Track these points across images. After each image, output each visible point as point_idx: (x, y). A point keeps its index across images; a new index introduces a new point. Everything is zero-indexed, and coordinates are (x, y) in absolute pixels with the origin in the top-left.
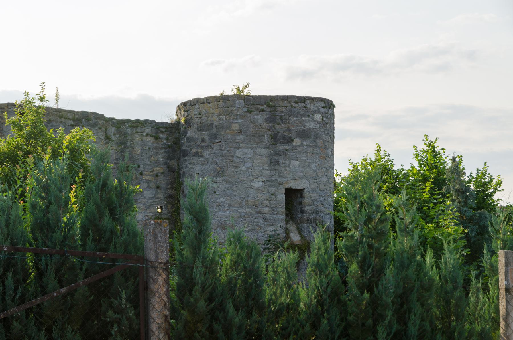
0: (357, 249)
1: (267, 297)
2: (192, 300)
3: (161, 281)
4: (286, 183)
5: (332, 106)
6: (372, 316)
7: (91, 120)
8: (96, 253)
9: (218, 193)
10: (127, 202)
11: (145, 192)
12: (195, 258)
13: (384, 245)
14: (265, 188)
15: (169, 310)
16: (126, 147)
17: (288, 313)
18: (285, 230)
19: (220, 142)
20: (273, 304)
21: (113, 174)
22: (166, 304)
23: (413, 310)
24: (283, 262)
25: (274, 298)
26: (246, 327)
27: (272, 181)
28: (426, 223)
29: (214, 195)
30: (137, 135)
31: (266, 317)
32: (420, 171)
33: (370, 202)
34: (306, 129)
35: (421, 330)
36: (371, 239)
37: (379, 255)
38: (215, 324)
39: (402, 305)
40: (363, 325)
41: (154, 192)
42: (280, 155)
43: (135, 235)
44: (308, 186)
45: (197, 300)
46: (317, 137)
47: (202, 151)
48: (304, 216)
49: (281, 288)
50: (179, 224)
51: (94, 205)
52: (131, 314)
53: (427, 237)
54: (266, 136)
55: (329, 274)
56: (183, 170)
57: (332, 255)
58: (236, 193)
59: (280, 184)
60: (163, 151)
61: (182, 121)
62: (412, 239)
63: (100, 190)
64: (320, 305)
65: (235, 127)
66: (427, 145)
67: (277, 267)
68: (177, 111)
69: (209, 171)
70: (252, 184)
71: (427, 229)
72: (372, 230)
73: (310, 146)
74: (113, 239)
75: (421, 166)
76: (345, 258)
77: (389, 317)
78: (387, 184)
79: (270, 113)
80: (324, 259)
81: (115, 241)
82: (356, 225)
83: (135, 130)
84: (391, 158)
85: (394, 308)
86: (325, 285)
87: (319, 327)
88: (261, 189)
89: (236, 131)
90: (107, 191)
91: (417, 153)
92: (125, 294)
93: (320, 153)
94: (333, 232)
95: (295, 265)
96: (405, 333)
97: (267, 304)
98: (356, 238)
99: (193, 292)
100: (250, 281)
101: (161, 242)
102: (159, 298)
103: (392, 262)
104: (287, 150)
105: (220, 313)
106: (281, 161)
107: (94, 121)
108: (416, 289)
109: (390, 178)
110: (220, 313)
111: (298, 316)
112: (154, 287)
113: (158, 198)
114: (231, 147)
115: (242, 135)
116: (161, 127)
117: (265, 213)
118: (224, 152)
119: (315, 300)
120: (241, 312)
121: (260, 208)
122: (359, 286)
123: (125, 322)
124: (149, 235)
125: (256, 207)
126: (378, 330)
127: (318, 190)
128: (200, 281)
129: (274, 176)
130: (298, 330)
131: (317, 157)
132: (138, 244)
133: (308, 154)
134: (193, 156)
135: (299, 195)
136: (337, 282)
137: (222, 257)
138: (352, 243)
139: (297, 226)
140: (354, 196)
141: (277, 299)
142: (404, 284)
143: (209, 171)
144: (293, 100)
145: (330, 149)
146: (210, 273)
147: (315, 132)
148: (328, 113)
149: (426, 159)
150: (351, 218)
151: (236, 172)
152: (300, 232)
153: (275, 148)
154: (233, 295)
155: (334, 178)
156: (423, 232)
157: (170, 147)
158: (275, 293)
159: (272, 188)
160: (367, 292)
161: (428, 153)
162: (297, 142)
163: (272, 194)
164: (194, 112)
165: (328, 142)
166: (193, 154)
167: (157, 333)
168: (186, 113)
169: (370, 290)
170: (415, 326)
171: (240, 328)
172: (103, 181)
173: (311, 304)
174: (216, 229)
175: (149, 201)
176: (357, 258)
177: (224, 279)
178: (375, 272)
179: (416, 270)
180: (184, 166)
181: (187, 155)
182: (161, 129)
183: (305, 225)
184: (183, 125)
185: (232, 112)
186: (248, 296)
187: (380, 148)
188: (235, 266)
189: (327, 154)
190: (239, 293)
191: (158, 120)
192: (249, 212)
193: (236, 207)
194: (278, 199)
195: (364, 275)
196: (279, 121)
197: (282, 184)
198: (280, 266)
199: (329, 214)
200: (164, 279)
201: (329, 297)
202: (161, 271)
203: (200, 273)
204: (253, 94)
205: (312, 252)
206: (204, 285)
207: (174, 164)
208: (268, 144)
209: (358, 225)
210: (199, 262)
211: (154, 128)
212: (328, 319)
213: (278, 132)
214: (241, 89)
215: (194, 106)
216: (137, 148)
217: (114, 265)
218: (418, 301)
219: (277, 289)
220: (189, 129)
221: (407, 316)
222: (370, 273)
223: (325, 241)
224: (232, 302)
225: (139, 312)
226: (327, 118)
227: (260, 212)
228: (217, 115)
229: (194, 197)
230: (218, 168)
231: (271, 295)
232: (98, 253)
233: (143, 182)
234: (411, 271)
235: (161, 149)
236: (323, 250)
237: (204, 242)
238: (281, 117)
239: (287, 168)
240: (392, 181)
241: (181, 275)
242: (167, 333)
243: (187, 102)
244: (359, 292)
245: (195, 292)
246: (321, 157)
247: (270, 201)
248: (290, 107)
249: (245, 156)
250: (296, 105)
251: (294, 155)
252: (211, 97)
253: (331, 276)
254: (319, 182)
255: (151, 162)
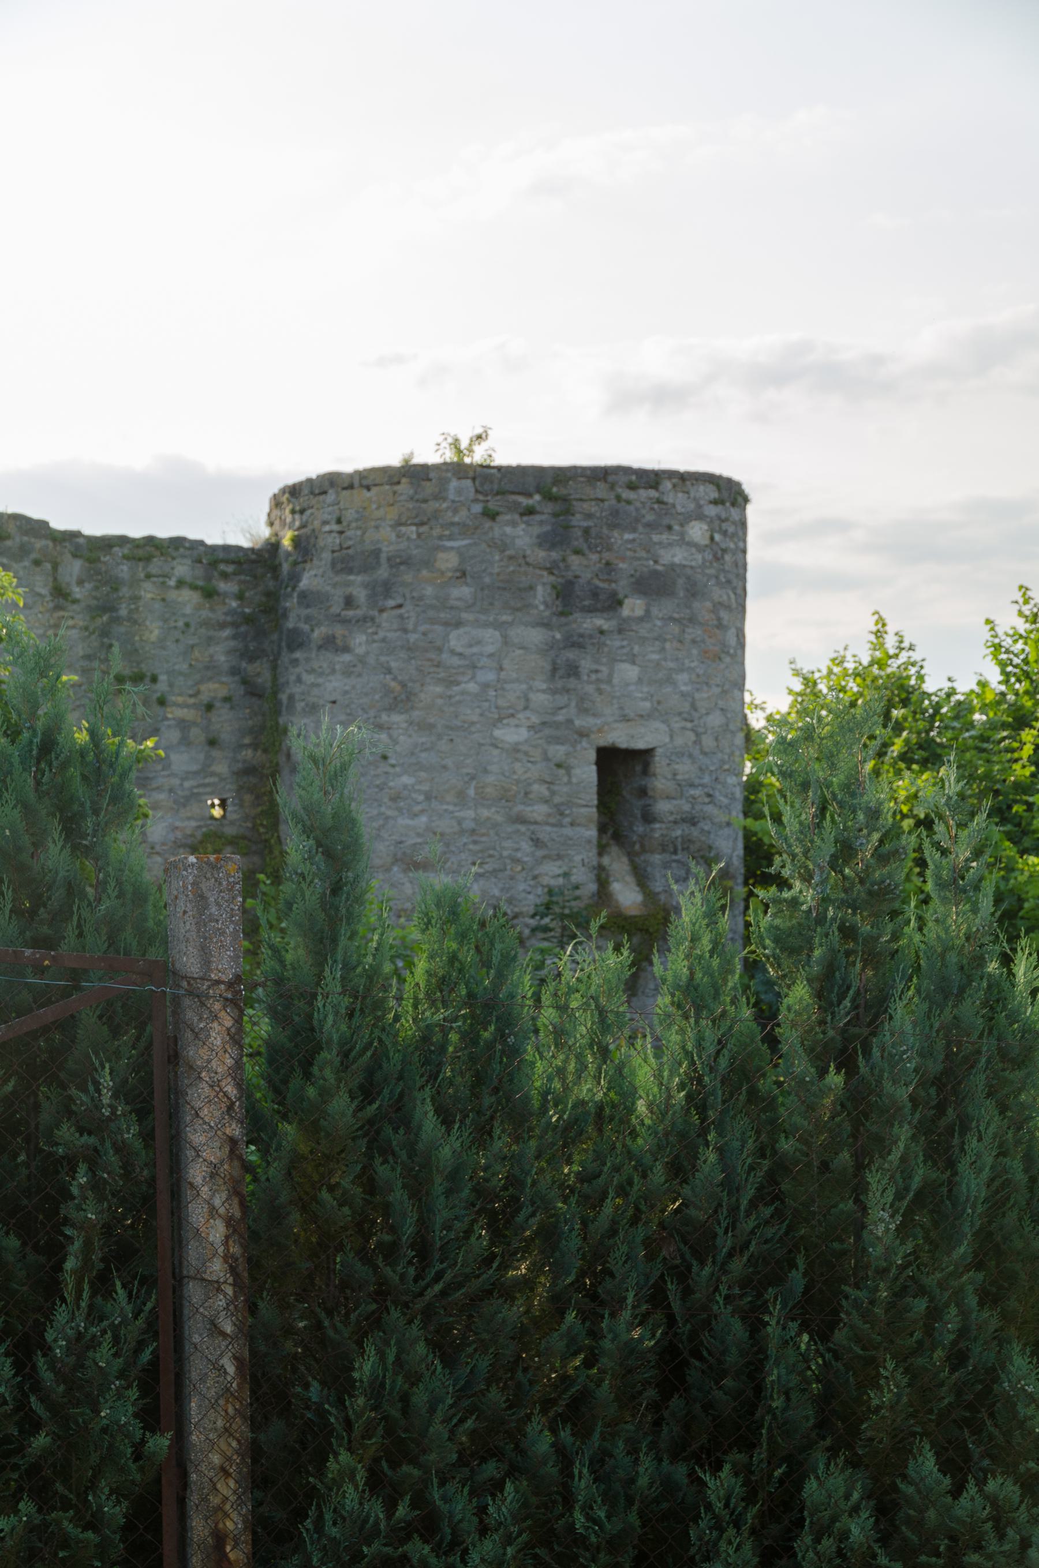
0: (809, 941)
1: (538, 1084)
2: (311, 1092)
3: (217, 1037)
4: (600, 731)
5: (740, 500)
6: (851, 1140)
7: (8, 537)
8: (23, 952)
9: (393, 761)
10: (115, 799)
11: (174, 757)
12: (320, 964)
13: (890, 927)
14: (535, 747)
15: (242, 1123)
16: (117, 620)
17: (600, 1130)
18: (595, 872)
19: (400, 606)
20: (556, 1105)
21: (78, 703)
22: (233, 1103)
23: (974, 1124)
24: (585, 979)
25: (557, 1085)
26: (474, 1171)
27: (557, 725)
28: (1022, 853)
29: (384, 767)
30: (148, 585)
31: (533, 1143)
32: (1003, 694)
33: (847, 799)
34: (659, 568)
35: (997, 1183)
36: (850, 911)
37: (872, 958)
38: (382, 1164)
39: (941, 1108)
40: (825, 1166)
41: (202, 756)
42: (581, 646)
43: (140, 897)
44: (667, 740)
45: (325, 1094)
46: (694, 592)
47: (346, 633)
48: (653, 830)
49: (580, 1057)
50: (276, 853)
51: (15, 806)
52: (130, 1132)
53: (1023, 896)
54: (540, 588)
55: (724, 1013)
56: (288, 691)
57: (733, 957)
58: (449, 762)
59: (583, 734)
60: (227, 632)
61: (286, 542)
62: (975, 910)
63: (33, 761)
64: (697, 1108)
65: (447, 561)
66: (1026, 617)
67: (568, 994)
68: (271, 510)
69: (366, 694)
70: (497, 733)
71: (1022, 870)
72: (853, 884)
73: (672, 619)
74: (75, 909)
75: (1007, 682)
76: (772, 966)
77: (901, 1145)
78: (905, 734)
79: (554, 520)
80: (708, 972)
81: (80, 917)
82: (806, 867)
83: (144, 569)
84: (916, 656)
85: (917, 1116)
86: (712, 1050)
87: (693, 1174)
88: (524, 748)
89: (450, 574)
90: (55, 763)
91: (997, 641)
92: (110, 1074)
93: (703, 641)
94: (740, 879)
95: (622, 987)
96: (950, 1191)
97: (536, 1104)
98: (804, 907)
99: (315, 1070)
100: (486, 1035)
101: (217, 921)
102: (212, 1086)
103: (915, 980)
104: (602, 632)
105: (396, 1130)
106: (586, 664)
107: (18, 539)
108: (984, 1060)
109: (914, 717)
110: (396, 1130)
111: (628, 1141)
112: (196, 1054)
113: (213, 774)
114: (433, 621)
115: (467, 584)
116: (223, 561)
117: (536, 823)
118: (413, 637)
119: (683, 1094)
120: (460, 1127)
121: (520, 807)
122: (812, 1050)
123: (112, 1158)
124: (182, 897)
125: (510, 804)
126: (868, 1183)
127: (696, 752)
128: (335, 1037)
129: (564, 711)
130: (630, 1182)
131: (695, 652)
132: (150, 924)
133: (668, 645)
134: (320, 647)
135: (639, 768)
136: (748, 1040)
137: (405, 954)
138: (794, 921)
139: (632, 862)
140: (800, 780)
141: (566, 1088)
142: (948, 1045)
143: (366, 694)
144: (623, 479)
145: (733, 631)
146: (367, 1011)
147: (688, 578)
148: (726, 520)
149: (1023, 660)
150: (790, 846)
151: (450, 697)
152: (642, 878)
153: (566, 624)
154: (436, 1078)
155: (745, 717)
156: (1012, 881)
157: (249, 620)
158: (561, 1072)
159: (558, 747)
160: (838, 1071)
161: (1029, 642)
162: (633, 606)
163: (559, 766)
164: (322, 513)
165: (728, 608)
166: (320, 643)
167: (205, 1190)
168: (297, 516)
169: (847, 1063)
170: (981, 1170)
171: (454, 1177)
172: (43, 734)
173: (668, 1106)
174: (388, 870)
175: (187, 784)
176: (807, 968)
177: (407, 1028)
178: (861, 1010)
179: (985, 1004)
180: (293, 678)
181: (301, 645)
182: (222, 567)
183: (657, 858)
184: (288, 554)
185: (436, 514)
186: (479, 1080)
187: (884, 625)
188: (441, 991)
189: (724, 645)
190: (452, 1070)
191: (213, 538)
192: (488, 818)
193: (448, 803)
194: (574, 780)
195: (829, 1018)
196: (580, 543)
197: (587, 736)
198: (578, 991)
199: (728, 824)
200: (228, 1029)
201: (723, 1082)
202: (217, 1006)
203: (337, 1013)
204: (502, 459)
205: (673, 950)
206: (348, 1047)
207: (260, 671)
208: (547, 613)
209: (811, 867)
210: (333, 978)
211: (200, 562)
212: (720, 1151)
213: (576, 577)
214: (464, 444)
215: (321, 498)
216: (148, 623)
217: (77, 988)
218: (989, 1095)
219: (566, 1061)
220: (308, 566)
221: (956, 1141)
222: (848, 1014)
223: (711, 916)
224: (433, 1099)
225: (153, 1128)
226: (725, 533)
227: (521, 820)
228: (391, 523)
229: (317, 783)
230: (393, 684)
231: (550, 1079)
232: (28, 952)
233: (169, 726)
234: (971, 1008)
235: (222, 626)
236: (706, 942)
237: (348, 919)
238: (586, 531)
239: (603, 686)
240: (921, 725)
241: (279, 1016)
242: (236, 1192)
243: (301, 484)
244: (813, 1070)
245: (321, 1070)
246: (706, 652)
247: (552, 787)
248: (614, 502)
249: (475, 650)
250: (626, 494)
251: (623, 647)
252: (373, 470)
253: (728, 1023)
254: (701, 730)
255: (191, 665)
